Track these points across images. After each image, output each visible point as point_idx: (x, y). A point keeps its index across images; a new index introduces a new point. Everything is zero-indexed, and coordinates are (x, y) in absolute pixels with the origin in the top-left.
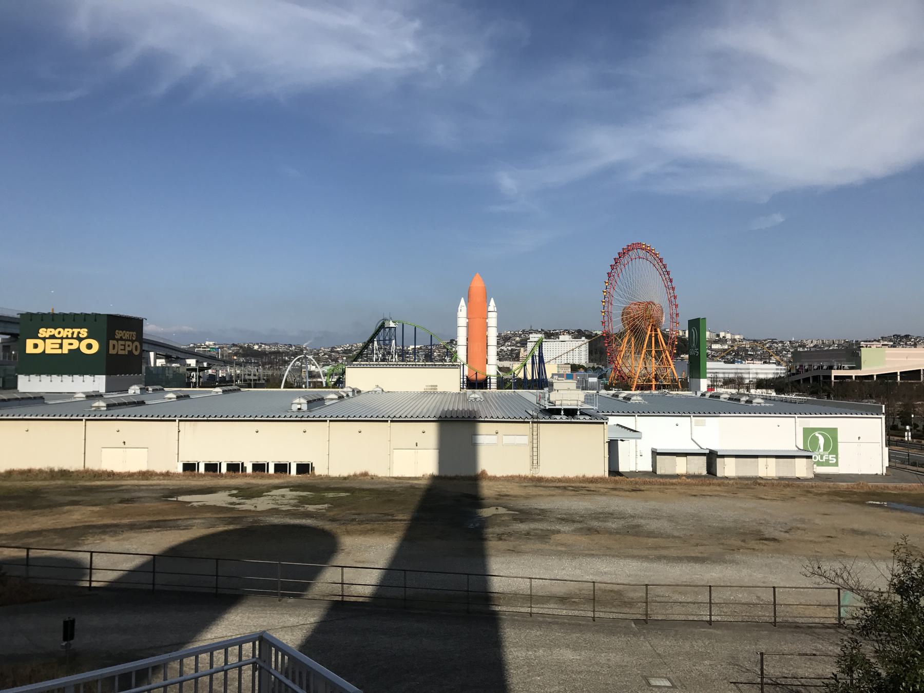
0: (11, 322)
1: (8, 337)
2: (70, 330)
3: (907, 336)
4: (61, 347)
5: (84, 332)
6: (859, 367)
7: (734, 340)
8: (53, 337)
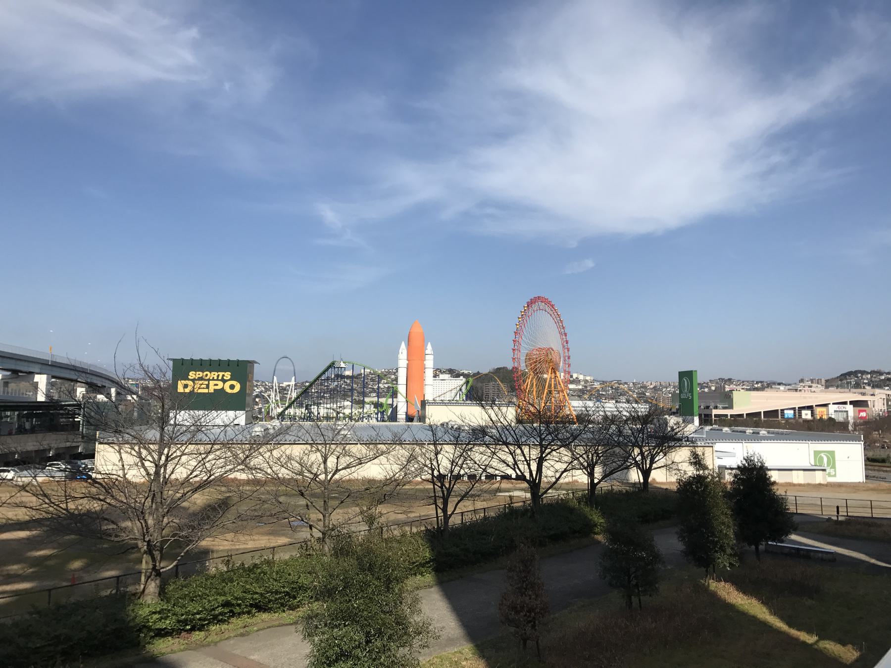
0: (25, 361)
1: (8, 373)
3: (730, 380)
4: (208, 387)
5: (228, 375)
6: (731, 407)
7: (586, 381)
8: (201, 379)
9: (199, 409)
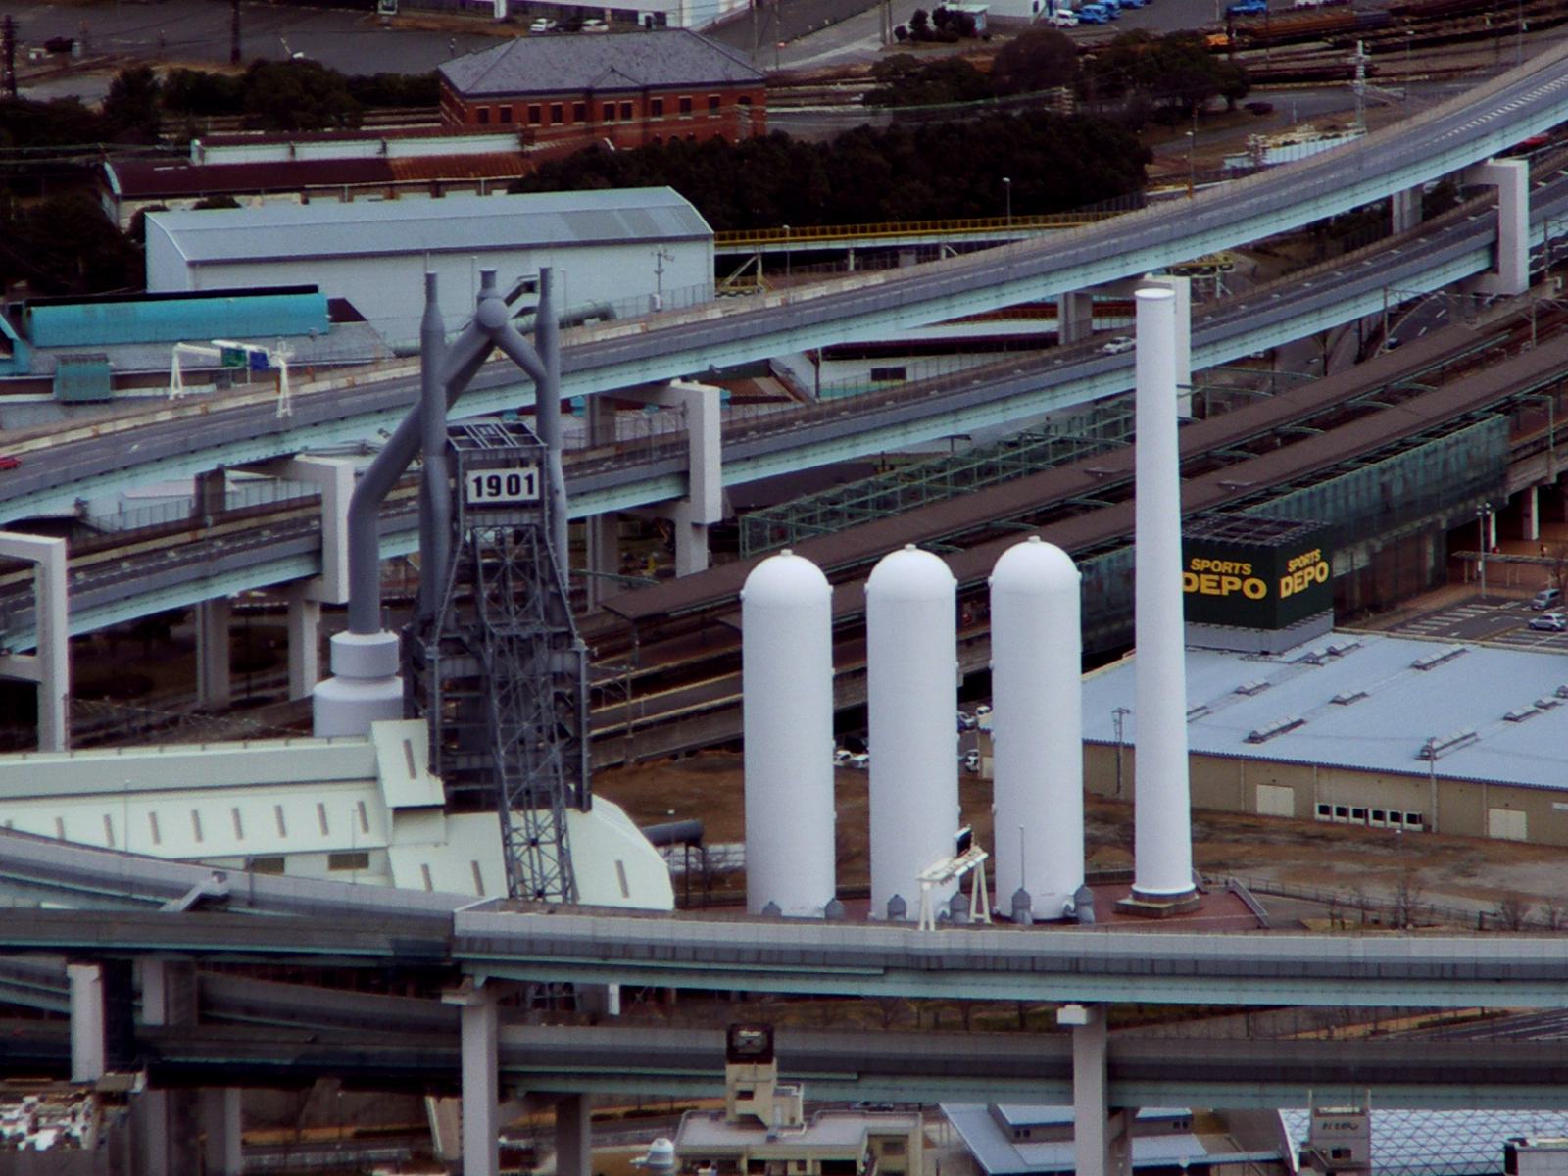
2: (1231, 564)
4: (1219, 586)
5: (1247, 569)
8: (1208, 571)
9: (350, 7)
